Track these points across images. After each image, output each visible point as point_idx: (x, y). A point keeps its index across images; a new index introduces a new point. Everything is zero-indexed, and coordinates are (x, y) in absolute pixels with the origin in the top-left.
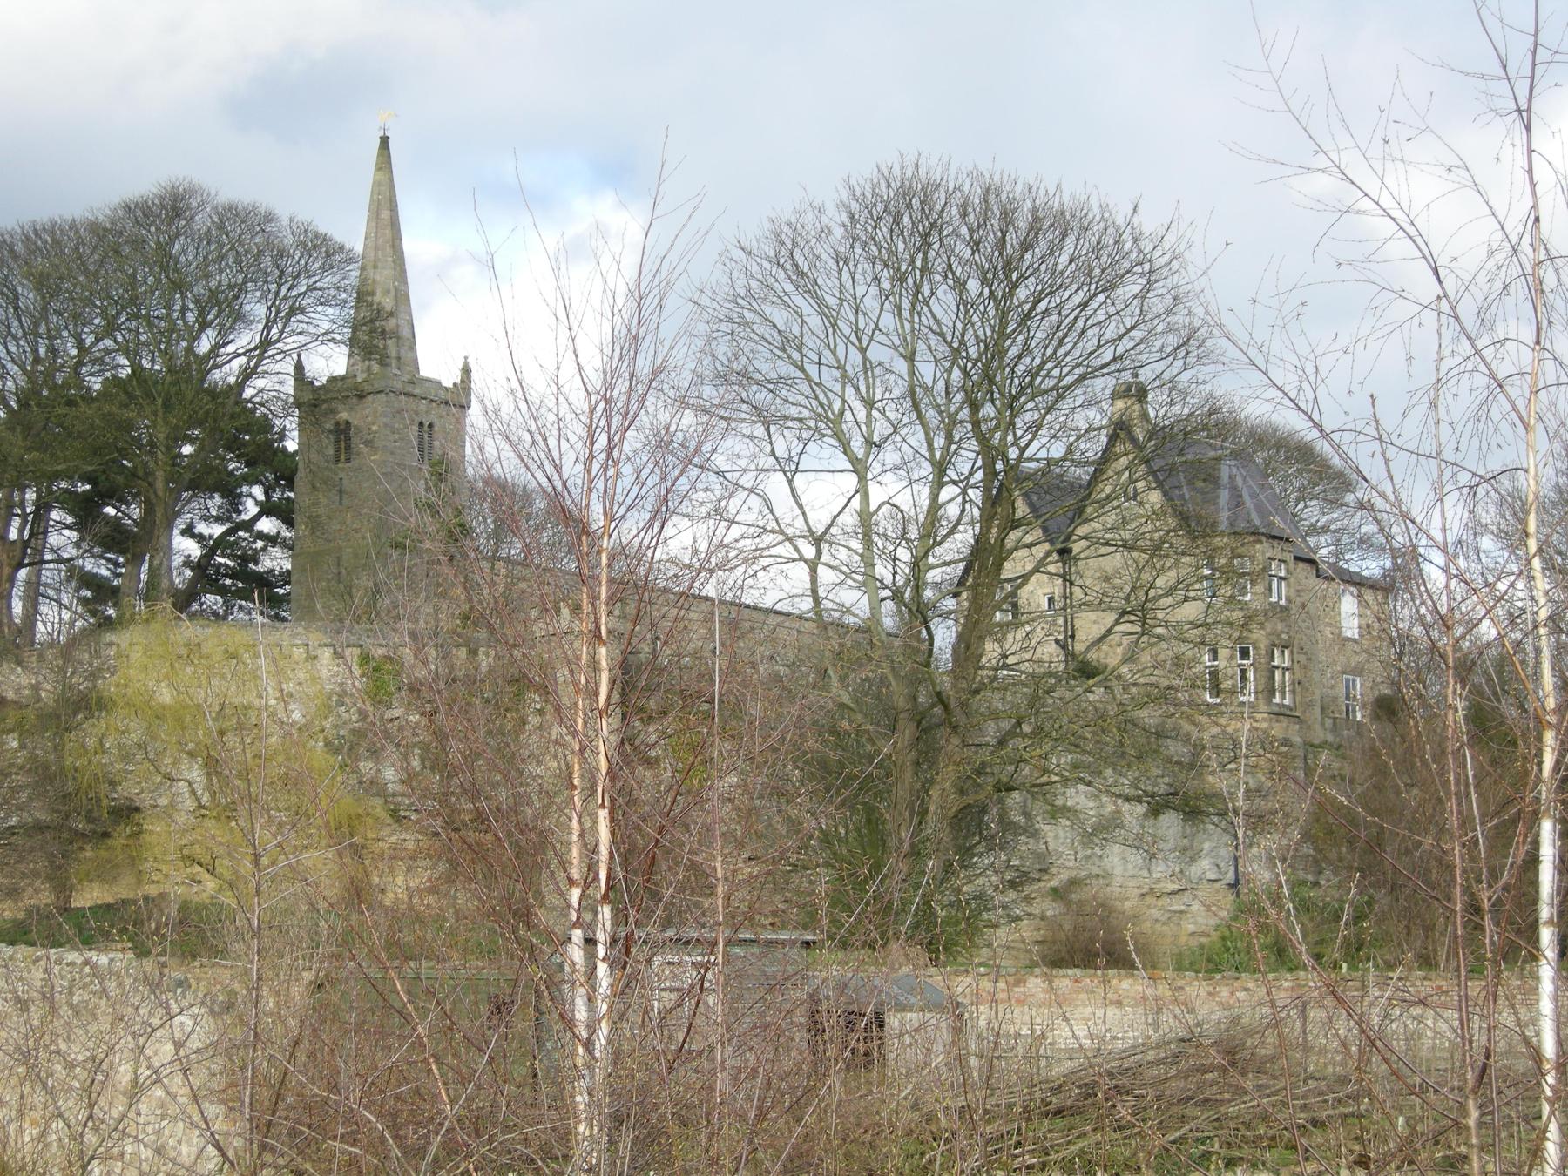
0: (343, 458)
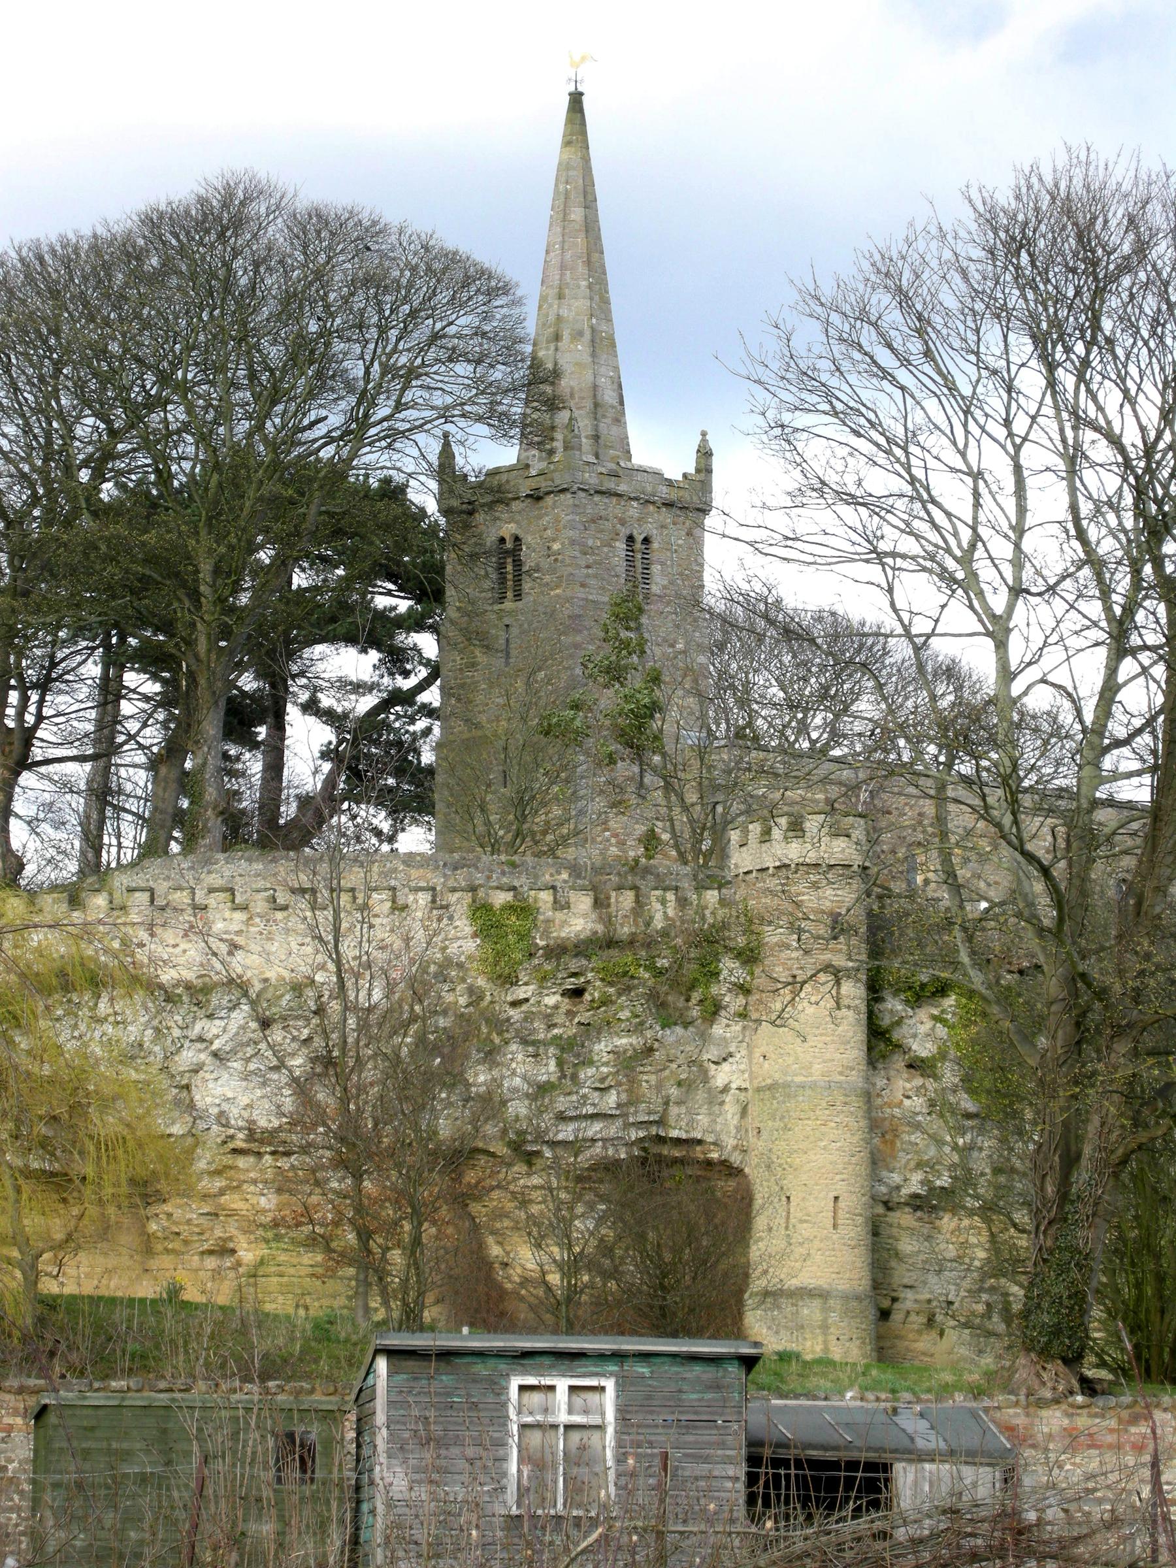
0: (510, 594)
